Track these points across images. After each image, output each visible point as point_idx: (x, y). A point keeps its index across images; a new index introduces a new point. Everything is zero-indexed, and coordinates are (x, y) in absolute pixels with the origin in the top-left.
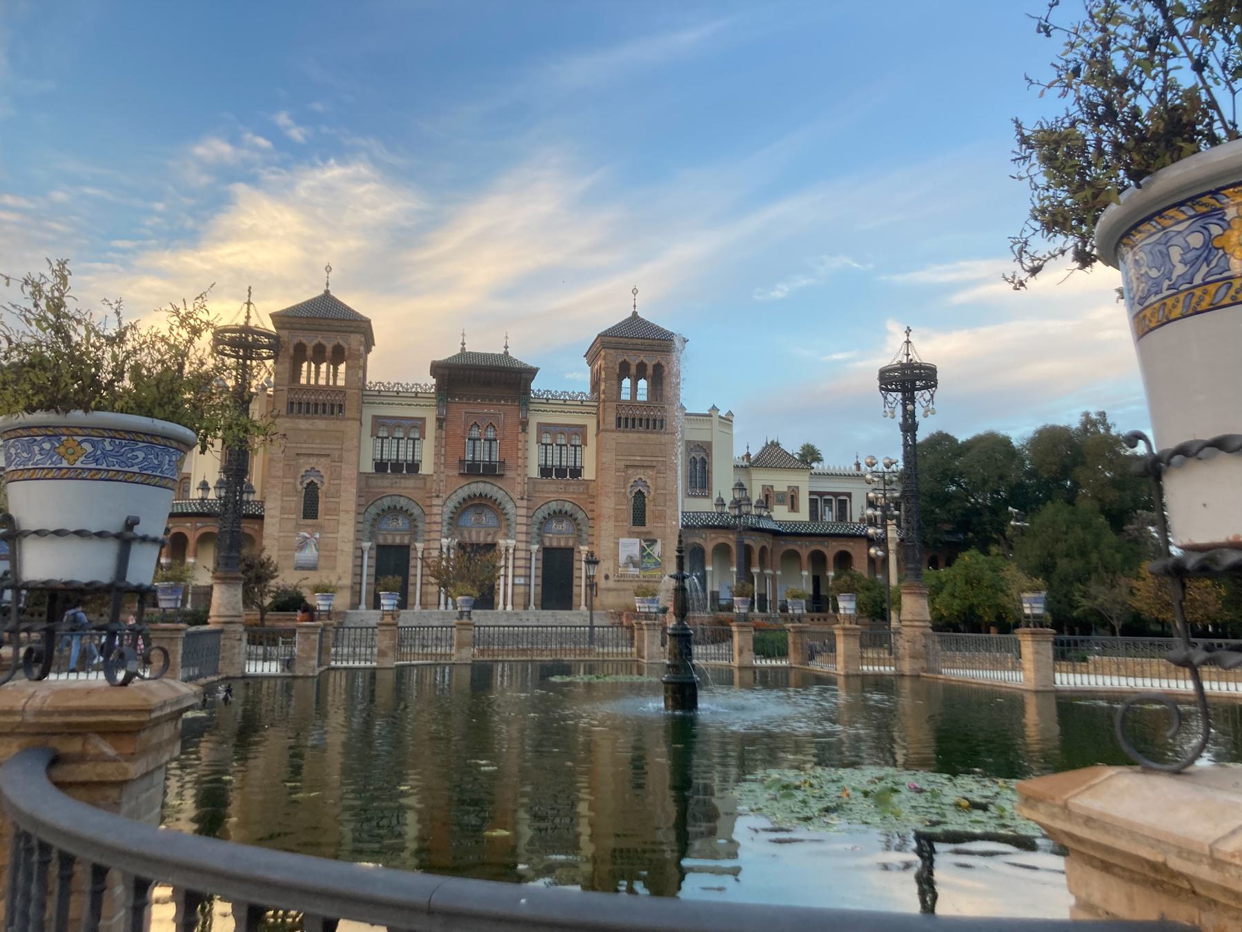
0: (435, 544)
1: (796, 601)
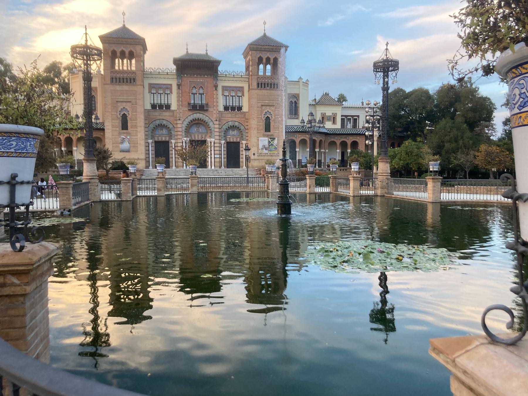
0: (179, 142)
1: (334, 165)
